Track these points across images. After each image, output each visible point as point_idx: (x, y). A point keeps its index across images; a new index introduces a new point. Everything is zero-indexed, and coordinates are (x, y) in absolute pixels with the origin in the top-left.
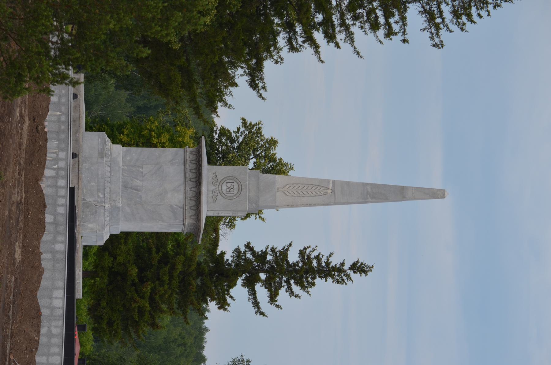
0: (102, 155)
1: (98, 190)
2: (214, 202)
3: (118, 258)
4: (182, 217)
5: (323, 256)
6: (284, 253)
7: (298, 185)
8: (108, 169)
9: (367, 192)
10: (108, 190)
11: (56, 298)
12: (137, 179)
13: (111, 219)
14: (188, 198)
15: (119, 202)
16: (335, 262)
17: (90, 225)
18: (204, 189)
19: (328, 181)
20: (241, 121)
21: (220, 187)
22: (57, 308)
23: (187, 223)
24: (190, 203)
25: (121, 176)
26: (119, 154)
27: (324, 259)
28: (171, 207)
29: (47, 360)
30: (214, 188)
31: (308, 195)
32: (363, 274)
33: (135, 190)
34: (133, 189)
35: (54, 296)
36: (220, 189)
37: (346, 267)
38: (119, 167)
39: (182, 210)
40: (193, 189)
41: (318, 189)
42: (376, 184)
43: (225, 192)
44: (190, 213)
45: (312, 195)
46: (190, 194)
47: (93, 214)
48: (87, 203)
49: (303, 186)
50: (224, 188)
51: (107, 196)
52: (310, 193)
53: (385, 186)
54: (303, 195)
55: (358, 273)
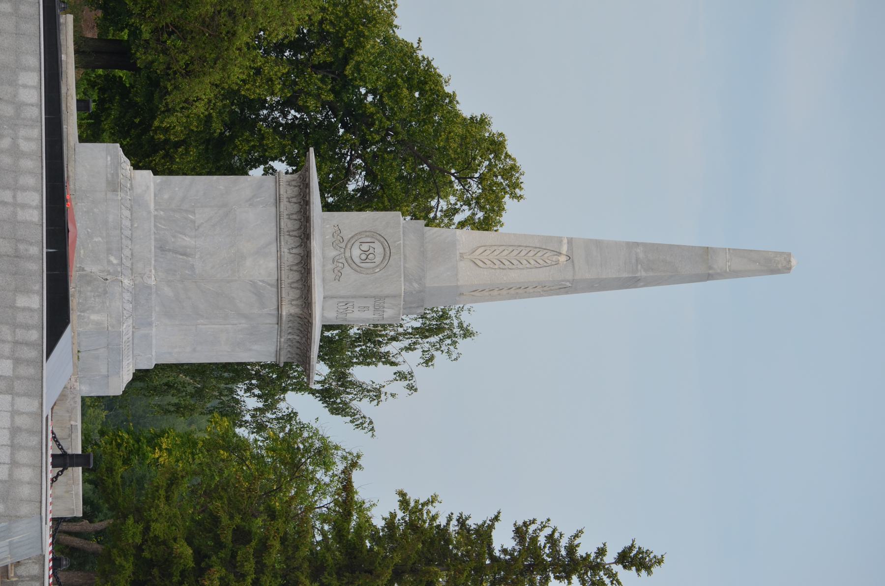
0: (114, 185)
1: (109, 251)
2: (338, 278)
3: (153, 525)
4: (276, 303)
5: (561, 535)
6: (484, 533)
7: (501, 249)
8: (127, 213)
9: (637, 260)
10: (127, 252)
11: (25, 86)
12: (185, 235)
13: (135, 308)
14: (285, 268)
15: (150, 277)
16: (586, 548)
17: (94, 317)
18: (316, 245)
19: (560, 240)
20: (398, 498)
21: (348, 251)
22: (27, 105)
23: (284, 313)
24: (290, 277)
25: (153, 229)
26: (148, 187)
27: (564, 542)
28: (253, 284)
29: (14, 197)
30: (335, 253)
31: (520, 266)
32: (643, 573)
33: (181, 254)
34: (176, 252)
35: (20, 82)
36: (348, 254)
37: (609, 558)
38: (149, 212)
39: (275, 290)
40: (294, 251)
41: (539, 254)
42: (653, 245)
43: (357, 261)
44: (290, 295)
45: (528, 266)
46: (289, 258)
47: (99, 296)
48: (86, 275)
49: (511, 249)
50: (356, 252)
51: (128, 263)
52: (525, 262)
53: (671, 247)
54: (511, 266)
55: (634, 568)
